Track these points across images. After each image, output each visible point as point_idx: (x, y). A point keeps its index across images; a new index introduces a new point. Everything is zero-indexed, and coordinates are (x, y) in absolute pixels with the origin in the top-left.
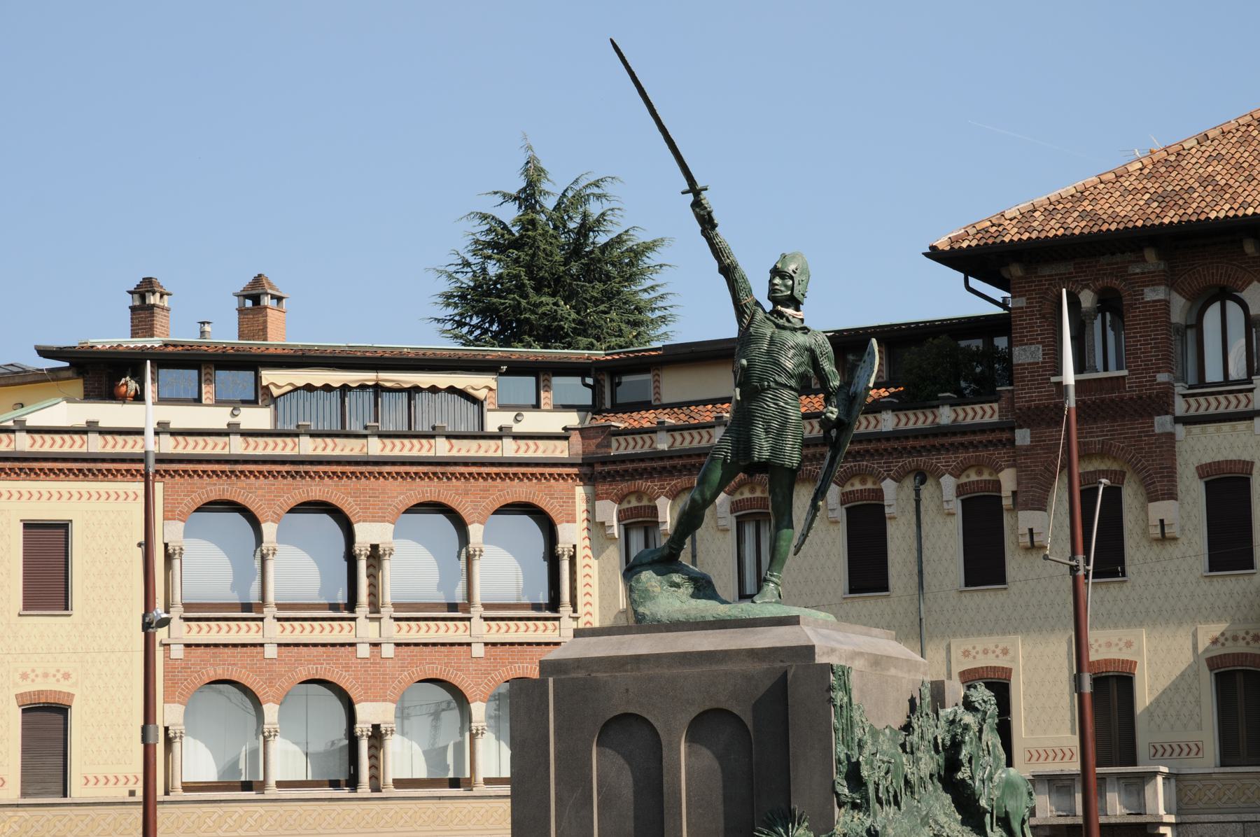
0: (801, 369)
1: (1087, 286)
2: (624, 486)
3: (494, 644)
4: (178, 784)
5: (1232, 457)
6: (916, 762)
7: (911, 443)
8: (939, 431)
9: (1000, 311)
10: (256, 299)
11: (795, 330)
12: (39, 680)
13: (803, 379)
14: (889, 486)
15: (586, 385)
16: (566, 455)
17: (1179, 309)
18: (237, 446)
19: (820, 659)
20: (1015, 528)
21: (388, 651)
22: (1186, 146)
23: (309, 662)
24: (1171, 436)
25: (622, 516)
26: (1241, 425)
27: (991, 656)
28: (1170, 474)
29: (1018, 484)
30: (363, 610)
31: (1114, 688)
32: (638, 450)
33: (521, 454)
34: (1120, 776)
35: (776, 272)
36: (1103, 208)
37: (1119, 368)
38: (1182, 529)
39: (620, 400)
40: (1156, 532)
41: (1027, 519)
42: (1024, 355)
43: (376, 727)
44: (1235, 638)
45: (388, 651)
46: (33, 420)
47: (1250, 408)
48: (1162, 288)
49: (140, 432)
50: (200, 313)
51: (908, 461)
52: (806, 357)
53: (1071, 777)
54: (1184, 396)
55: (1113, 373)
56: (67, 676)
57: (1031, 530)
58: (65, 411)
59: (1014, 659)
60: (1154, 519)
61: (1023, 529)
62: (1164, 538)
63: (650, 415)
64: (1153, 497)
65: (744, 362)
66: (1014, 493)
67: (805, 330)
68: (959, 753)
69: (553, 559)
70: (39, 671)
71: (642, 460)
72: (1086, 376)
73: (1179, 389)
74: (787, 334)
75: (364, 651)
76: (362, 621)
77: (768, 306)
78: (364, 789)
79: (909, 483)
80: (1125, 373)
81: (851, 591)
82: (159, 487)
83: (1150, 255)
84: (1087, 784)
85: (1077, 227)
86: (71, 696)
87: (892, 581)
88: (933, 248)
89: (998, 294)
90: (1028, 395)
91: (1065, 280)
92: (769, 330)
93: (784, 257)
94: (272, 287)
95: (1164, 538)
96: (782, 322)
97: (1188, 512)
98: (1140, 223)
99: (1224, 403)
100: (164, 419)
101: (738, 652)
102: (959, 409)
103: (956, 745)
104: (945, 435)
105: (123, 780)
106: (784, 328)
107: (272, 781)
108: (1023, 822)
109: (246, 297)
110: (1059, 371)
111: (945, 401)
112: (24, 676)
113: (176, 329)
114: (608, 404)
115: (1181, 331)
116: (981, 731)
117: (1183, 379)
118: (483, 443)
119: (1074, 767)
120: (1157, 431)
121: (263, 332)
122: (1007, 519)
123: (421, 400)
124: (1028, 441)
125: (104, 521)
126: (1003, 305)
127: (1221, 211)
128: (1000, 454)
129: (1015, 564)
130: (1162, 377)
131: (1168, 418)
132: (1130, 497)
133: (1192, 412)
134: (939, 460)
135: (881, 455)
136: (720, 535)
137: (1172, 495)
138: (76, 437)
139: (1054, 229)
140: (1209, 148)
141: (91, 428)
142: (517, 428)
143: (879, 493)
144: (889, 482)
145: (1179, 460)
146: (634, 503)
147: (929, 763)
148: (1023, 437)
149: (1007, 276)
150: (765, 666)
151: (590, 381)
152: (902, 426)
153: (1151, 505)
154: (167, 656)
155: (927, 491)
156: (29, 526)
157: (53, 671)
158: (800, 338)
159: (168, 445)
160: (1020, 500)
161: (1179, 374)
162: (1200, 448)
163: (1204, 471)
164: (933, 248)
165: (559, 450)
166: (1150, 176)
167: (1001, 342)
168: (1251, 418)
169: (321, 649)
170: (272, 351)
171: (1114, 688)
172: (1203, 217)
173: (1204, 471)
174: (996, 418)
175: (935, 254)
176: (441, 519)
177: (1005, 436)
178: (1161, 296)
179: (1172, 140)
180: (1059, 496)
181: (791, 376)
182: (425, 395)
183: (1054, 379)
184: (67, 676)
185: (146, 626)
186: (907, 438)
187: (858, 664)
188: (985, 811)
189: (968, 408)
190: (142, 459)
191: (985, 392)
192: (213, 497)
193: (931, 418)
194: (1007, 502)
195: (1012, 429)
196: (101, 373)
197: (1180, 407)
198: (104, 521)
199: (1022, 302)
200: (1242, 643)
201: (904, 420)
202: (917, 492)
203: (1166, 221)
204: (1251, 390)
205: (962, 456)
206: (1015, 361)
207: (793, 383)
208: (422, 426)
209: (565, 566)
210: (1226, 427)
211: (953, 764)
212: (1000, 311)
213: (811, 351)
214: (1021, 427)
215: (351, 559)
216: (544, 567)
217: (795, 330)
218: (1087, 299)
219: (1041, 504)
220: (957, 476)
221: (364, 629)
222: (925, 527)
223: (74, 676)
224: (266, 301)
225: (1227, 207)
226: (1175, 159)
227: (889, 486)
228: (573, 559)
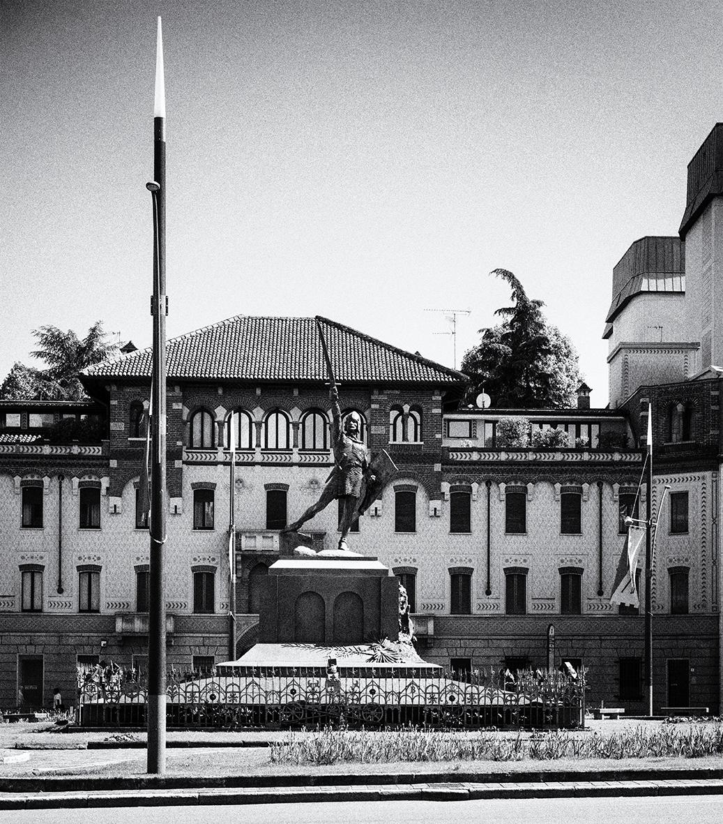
12: (202, 561)
14: (475, 486)
24: (181, 469)
27: (34, 559)
28: (180, 487)
29: (110, 484)
37: (421, 441)
40: (173, 511)
41: (114, 500)
44: (89, 558)
47: (328, 462)
54: (187, 452)
55: (419, 443)
57: (115, 506)
60: (172, 506)
70: (458, 559)
79: (55, 478)
80: (422, 443)
81: (452, 530)
87: (473, 527)
95: (115, 513)
99: (204, 457)
111: (75, 444)
124: (111, 466)
128: (102, 470)
131: (181, 461)
132: (420, 497)
134: (73, 471)
135: (43, 466)
143: (581, 490)
148: (114, 463)
155: (65, 482)
168: (292, 466)
173: (193, 485)
178: (181, 408)
180: (130, 492)
184: (99, 558)
186: (56, 459)
189: (87, 448)
191: (97, 443)
193: (68, 450)
194: (103, 492)
197: (185, 456)
202: (60, 483)
214: (112, 459)
227: (46, 480)
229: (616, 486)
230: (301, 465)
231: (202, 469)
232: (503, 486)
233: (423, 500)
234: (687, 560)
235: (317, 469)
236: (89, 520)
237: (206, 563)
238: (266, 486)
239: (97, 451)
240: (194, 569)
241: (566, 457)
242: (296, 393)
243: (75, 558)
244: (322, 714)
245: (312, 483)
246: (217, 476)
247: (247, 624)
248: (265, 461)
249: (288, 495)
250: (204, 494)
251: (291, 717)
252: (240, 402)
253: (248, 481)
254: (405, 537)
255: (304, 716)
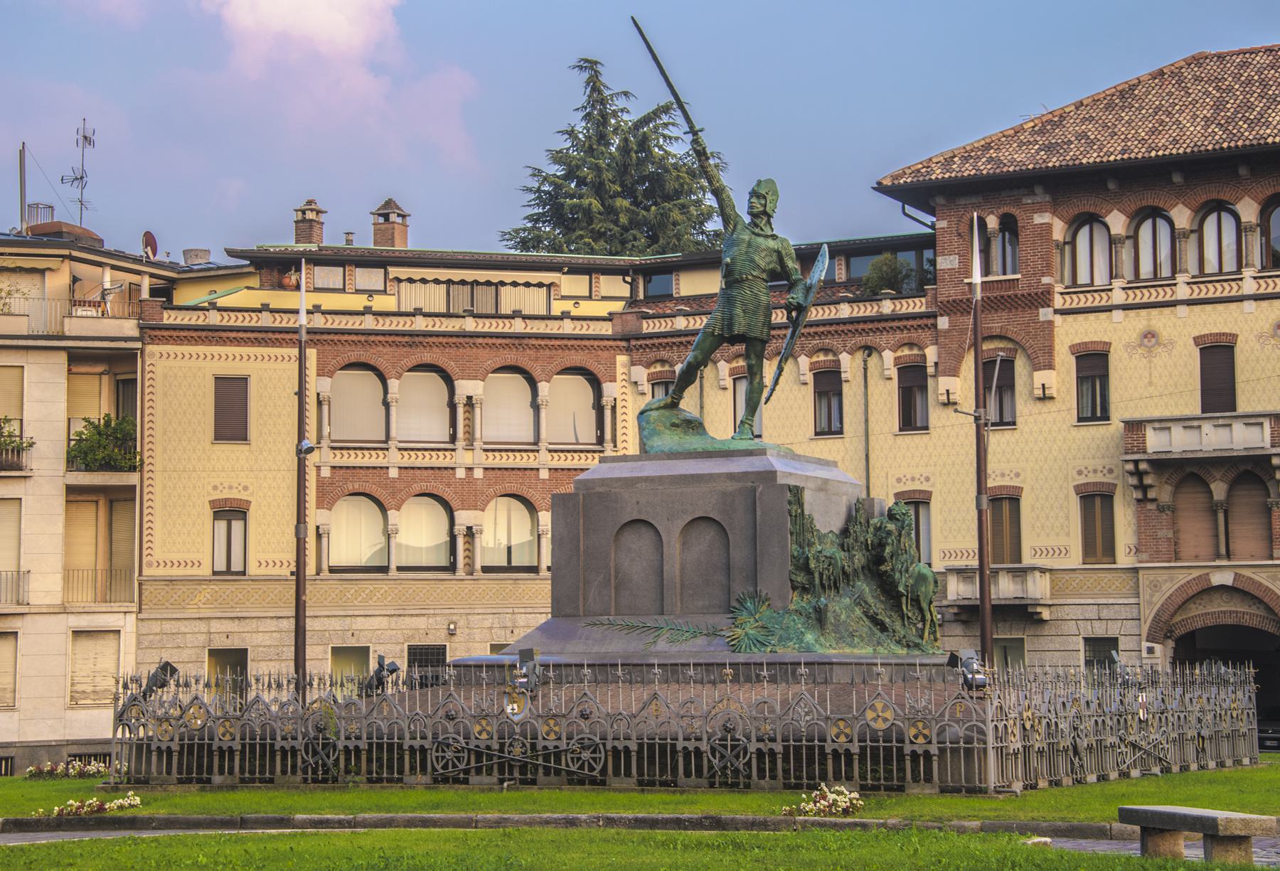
0: (771, 266)
1: (992, 213)
2: (652, 355)
3: (556, 469)
4: (325, 567)
5: (1096, 339)
6: (851, 558)
7: (861, 326)
8: (881, 318)
9: (930, 231)
10: (386, 217)
11: (767, 237)
13: (773, 275)
14: (844, 358)
15: (625, 281)
16: (610, 332)
17: (1059, 230)
18: (369, 323)
19: (781, 481)
20: (936, 388)
21: (478, 474)
22: (1067, 110)
23: (422, 480)
24: (1051, 323)
25: (650, 378)
26: (1167, 311)
28: (1050, 350)
30: (460, 444)
31: (1006, 506)
32: (662, 329)
33: (577, 332)
34: (1009, 571)
35: (754, 194)
36: (1004, 155)
37: (1014, 272)
38: (1058, 391)
39: (650, 293)
40: (1039, 393)
41: (944, 383)
42: (946, 263)
43: (469, 528)
44: (1095, 471)
45: (478, 474)
46: (221, 302)
47: (1240, 293)
48: (1047, 214)
49: (296, 312)
50: (349, 225)
51: (861, 340)
52: (775, 257)
53: (973, 570)
56: (246, 488)
58: (244, 295)
59: (1024, 481)
60: (1037, 384)
61: (942, 390)
62: (1045, 398)
63: (671, 305)
64: (1036, 367)
65: (728, 260)
66: (936, 364)
67: (774, 237)
68: (884, 551)
69: (599, 408)
70: (226, 485)
71: (665, 337)
72: (990, 278)
73: (1059, 288)
74: (760, 240)
75: (461, 473)
76: (460, 452)
77: (747, 219)
78: (461, 573)
80: (1018, 276)
82: (312, 353)
83: (1038, 190)
84: (984, 575)
85: (985, 168)
86: (249, 502)
88: (879, 183)
89: (929, 219)
90: (947, 292)
91: (976, 207)
92: (746, 236)
93: (759, 182)
94: (399, 208)
96: (757, 230)
97: (1061, 378)
98: (1031, 167)
100: (317, 303)
101: (719, 475)
102: (897, 302)
103: (882, 545)
104: (886, 320)
105: (286, 564)
106: (758, 235)
107: (393, 566)
108: (931, 602)
109: (380, 215)
110: (969, 273)
112: (1080, 473)
113: (331, 238)
114: (641, 296)
115: (1060, 247)
116: (900, 535)
117: (1062, 281)
118: (549, 322)
119: (975, 563)
120: (1042, 319)
121: (392, 242)
122: (930, 381)
123: (504, 291)
125: (270, 376)
126: (933, 226)
127: (1092, 158)
128: (924, 336)
129: (937, 417)
130: (1046, 280)
131: (1051, 310)
132: (1020, 365)
133: (1067, 306)
136: (721, 392)
137: (1050, 366)
138: (253, 315)
139: (968, 170)
140: (1083, 112)
141: (265, 308)
142: (574, 312)
144: (844, 354)
145: (1057, 341)
146: (659, 368)
147: (859, 558)
148: (943, 323)
149: (932, 204)
150: (739, 485)
151: (628, 279)
152: (855, 314)
153: (1036, 374)
154: (318, 475)
155: (873, 361)
156: (218, 379)
157: (235, 485)
158: (771, 244)
159: (319, 322)
160: (941, 368)
161: (1058, 278)
162: (1071, 333)
163: (1074, 349)
164: (879, 183)
165: (606, 329)
166: (1037, 133)
167: (928, 254)
169: (431, 472)
170: (397, 254)
171: (1006, 506)
172: (1077, 162)
173: (1074, 349)
174: (923, 309)
175: (880, 188)
176: (518, 377)
177: (930, 322)
179: (1055, 106)
180: (968, 365)
181: (764, 271)
182: (508, 287)
183: (966, 281)
184: (246, 488)
185: (299, 452)
187: (811, 485)
188: (902, 595)
190: (295, 331)
191: (920, 293)
192: (353, 360)
193: (876, 308)
194: (930, 370)
195: (935, 317)
196: (274, 267)
197: (1058, 302)
198: (270, 376)
199: (942, 224)
200: (1100, 475)
201: (856, 310)
202: (865, 362)
203: (1050, 165)
204: (1241, 279)
205: (899, 335)
206: (938, 267)
207: (764, 276)
208: (506, 309)
209: (608, 413)
210: (1092, 316)
211: (880, 560)
212: (930, 231)
213: (778, 252)
215: (452, 407)
216: (593, 414)
217: (767, 237)
218: (992, 222)
219: (954, 372)
220: (895, 351)
221: (462, 458)
222: (872, 386)
223: (251, 488)
224: (393, 217)
225: (1095, 155)
226: (1057, 120)
228: (614, 408)
229: (888, 356)
230: (1126, 307)
231: (1098, 319)
232: (804, 361)
233: (1025, 372)
234: (1017, 475)
235: (1154, 312)
236: (911, 420)
237: (1099, 478)
238: (1197, 340)
239: (917, 306)
240: (1078, 489)
241: (899, 306)
242: (1243, 171)
243: (892, 481)
244: (500, 757)
245: (1145, 336)
246: (1116, 331)
247: (1172, 579)
248: (1130, 301)
249: (1237, 350)
250: (1093, 365)
251: (447, 764)
252: (1150, 200)
253: (1165, 334)
254: (913, 441)
255: (469, 763)
